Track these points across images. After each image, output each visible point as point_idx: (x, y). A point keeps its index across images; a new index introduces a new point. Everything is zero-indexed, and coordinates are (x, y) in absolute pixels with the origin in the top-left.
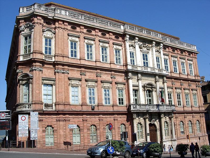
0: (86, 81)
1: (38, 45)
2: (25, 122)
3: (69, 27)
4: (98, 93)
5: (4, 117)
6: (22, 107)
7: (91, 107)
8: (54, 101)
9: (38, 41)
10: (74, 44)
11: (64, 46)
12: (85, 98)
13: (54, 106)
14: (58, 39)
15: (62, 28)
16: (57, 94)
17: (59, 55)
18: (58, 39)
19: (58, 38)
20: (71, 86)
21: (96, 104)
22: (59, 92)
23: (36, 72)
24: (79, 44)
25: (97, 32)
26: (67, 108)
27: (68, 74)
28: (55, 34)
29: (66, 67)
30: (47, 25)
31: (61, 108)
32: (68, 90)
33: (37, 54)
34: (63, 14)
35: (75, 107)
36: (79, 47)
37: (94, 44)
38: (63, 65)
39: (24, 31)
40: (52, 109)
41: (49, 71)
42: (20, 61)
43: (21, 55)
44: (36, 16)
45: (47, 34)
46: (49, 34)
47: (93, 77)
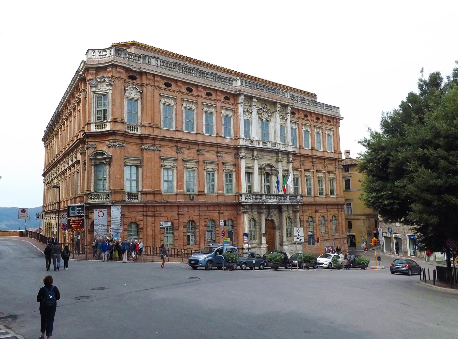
8: (140, 189)
17: (147, 125)
26: (158, 199)
31: (149, 198)
41: (134, 147)
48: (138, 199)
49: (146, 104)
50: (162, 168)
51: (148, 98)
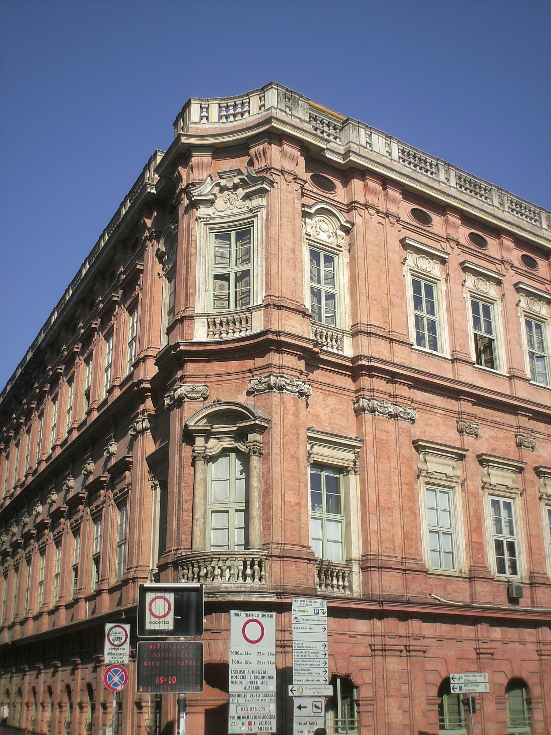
0: (482, 461)
1: (287, 272)
2: (259, 654)
3: (405, 209)
4: (528, 525)
5: (166, 619)
6: (190, 575)
7: (503, 588)
8: (357, 552)
9: (286, 254)
10: (423, 290)
11: (388, 293)
12: (481, 543)
13: (357, 578)
14: (366, 257)
15: (378, 212)
16: (373, 518)
17: (373, 330)
18: (366, 257)
19: (366, 254)
20: (426, 483)
21: (524, 575)
22: (378, 505)
23: (282, 400)
24: (444, 292)
25: (508, 249)
26: (417, 589)
27: (413, 421)
28: (347, 231)
29: (403, 391)
30: (315, 190)
31: (390, 584)
32: (413, 498)
33: (284, 312)
34: (378, 149)
35: (445, 587)
36: (445, 307)
37: (499, 301)
38: (393, 377)
39: (211, 202)
40: (348, 592)
41: (332, 401)
42: (194, 340)
43: (199, 315)
44: (276, 137)
45: (318, 230)
46: (324, 231)
47: (504, 448)
48: (351, 588)
49: (366, 266)
50: (422, 480)
51: (369, 246)
